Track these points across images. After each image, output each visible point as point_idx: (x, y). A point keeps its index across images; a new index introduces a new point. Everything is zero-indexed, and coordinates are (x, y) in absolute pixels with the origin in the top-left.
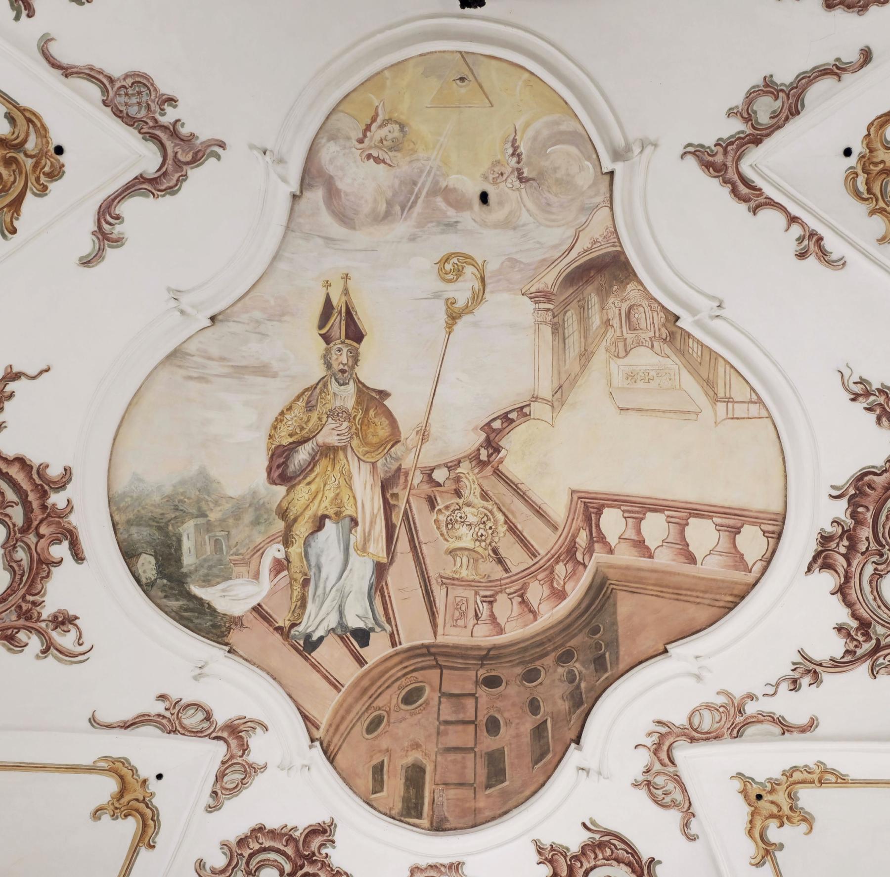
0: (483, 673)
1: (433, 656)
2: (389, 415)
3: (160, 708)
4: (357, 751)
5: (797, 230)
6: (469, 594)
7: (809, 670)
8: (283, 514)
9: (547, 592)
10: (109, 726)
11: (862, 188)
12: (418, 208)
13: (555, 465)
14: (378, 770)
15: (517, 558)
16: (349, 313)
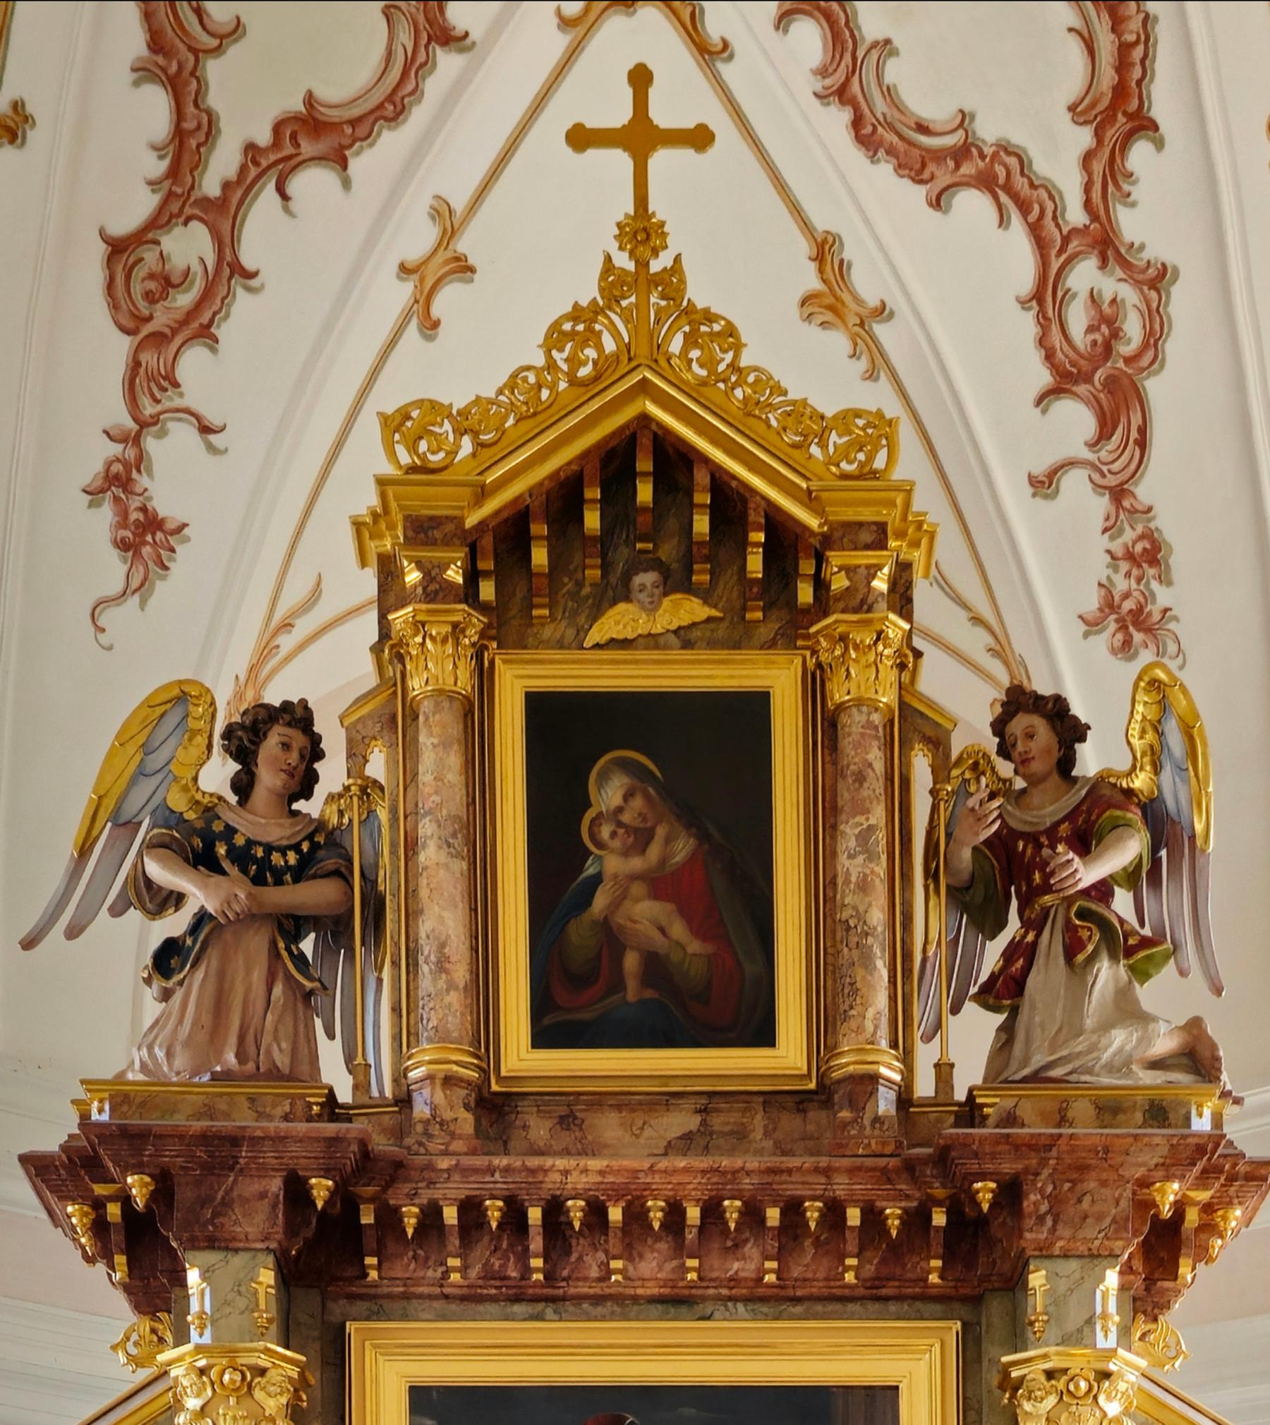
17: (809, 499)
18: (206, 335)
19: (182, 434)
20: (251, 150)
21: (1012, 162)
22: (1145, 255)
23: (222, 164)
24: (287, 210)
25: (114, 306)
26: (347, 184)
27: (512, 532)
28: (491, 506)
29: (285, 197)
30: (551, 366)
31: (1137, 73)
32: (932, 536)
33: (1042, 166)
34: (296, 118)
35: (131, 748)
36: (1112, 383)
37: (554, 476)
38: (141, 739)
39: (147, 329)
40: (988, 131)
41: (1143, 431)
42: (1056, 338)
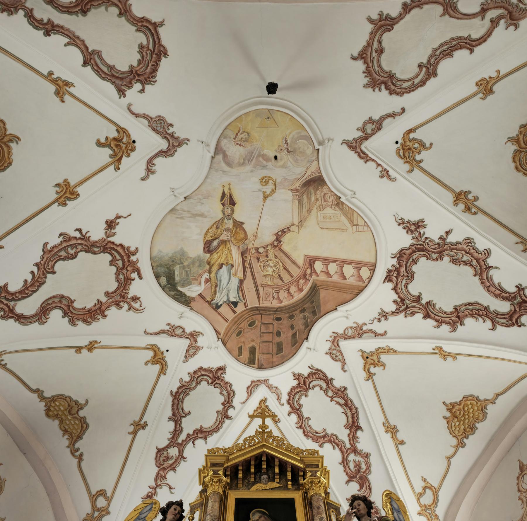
0: (275, 316)
1: (259, 310)
2: (244, 230)
3: (167, 328)
4: (233, 342)
5: (380, 169)
6: (271, 290)
7: (384, 315)
8: (209, 263)
9: (297, 289)
10: (151, 334)
11: (402, 154)
12: (254, 161)
13: (300, 246)
14: (240, 349)
15: (287, 278)
16: (231, 196)
17: (301, 461)
18: (174, 469)
19: (165, 489)
20: (188, 434)
21: (334, 437)
22: (363, 452)
23: (183, 437)
24: (194, 447)
25: (156, 462)
26: (206, 443)
27: (234, 469)
28: (230, 464)
29: (194, 444)
30: (245, 443)
31: (356, 418)
32: (329, 473)
33: (340, 437)
34: (198, 430)
35: (137, 512)
36: (361, 477)
37: (244, 460)
38: (140, 511)
39: (162, 467)
40: (329, 432)
41: (369, 486)
42: (348, 470)
